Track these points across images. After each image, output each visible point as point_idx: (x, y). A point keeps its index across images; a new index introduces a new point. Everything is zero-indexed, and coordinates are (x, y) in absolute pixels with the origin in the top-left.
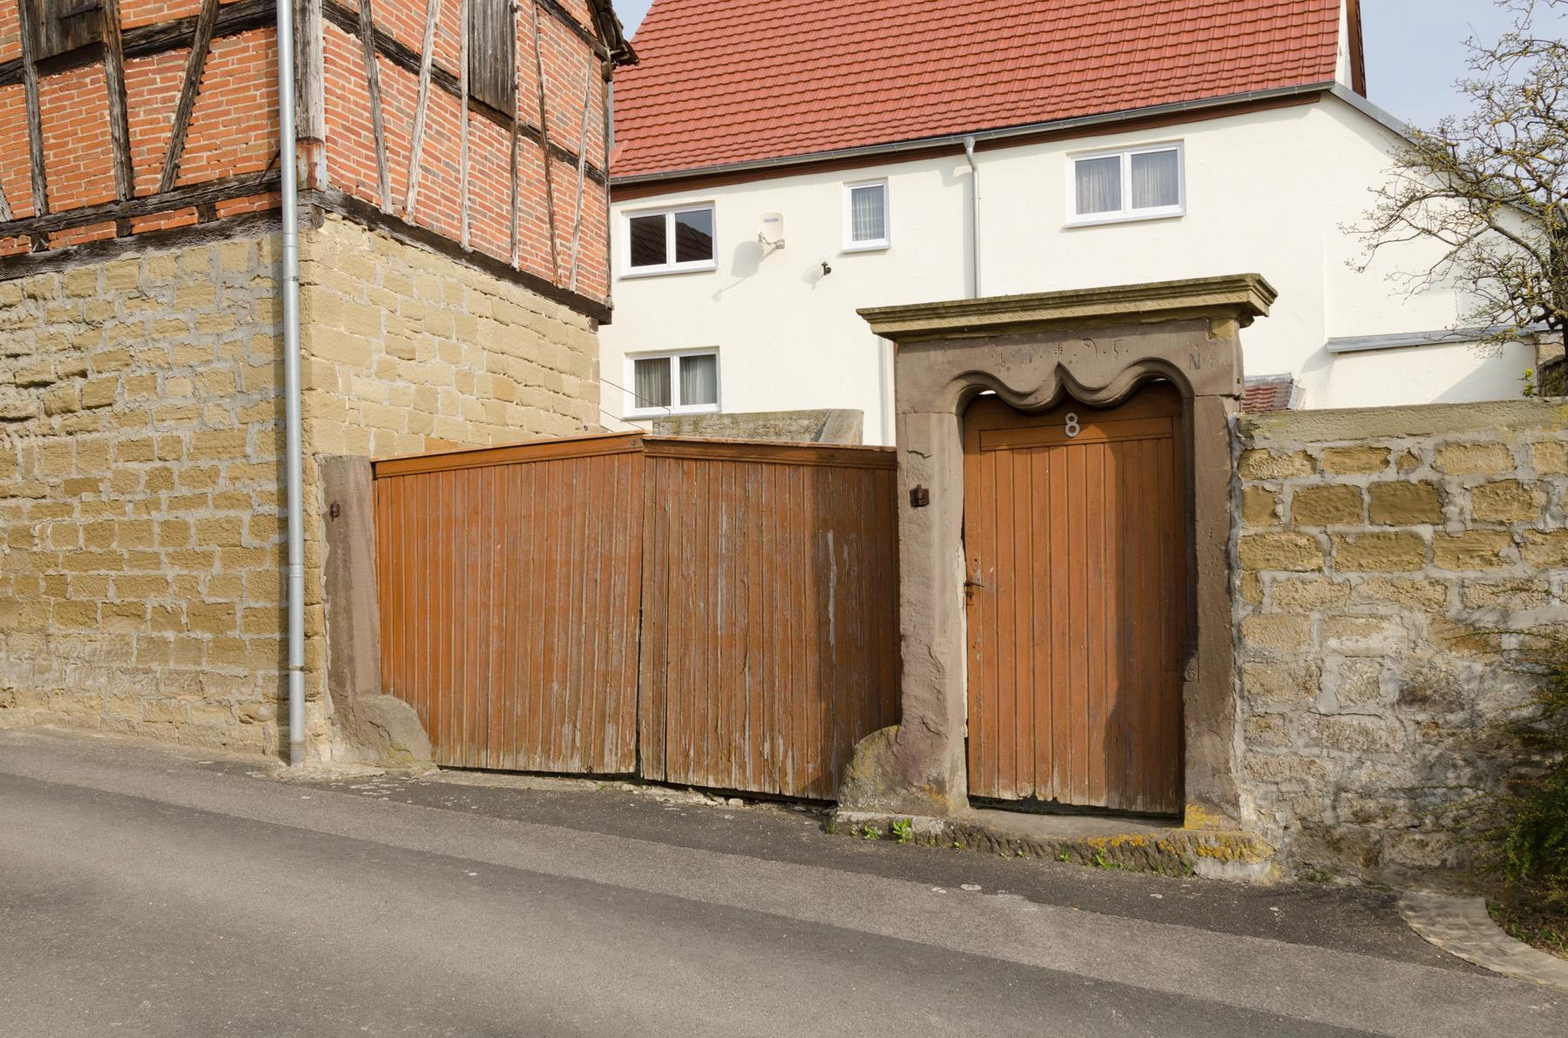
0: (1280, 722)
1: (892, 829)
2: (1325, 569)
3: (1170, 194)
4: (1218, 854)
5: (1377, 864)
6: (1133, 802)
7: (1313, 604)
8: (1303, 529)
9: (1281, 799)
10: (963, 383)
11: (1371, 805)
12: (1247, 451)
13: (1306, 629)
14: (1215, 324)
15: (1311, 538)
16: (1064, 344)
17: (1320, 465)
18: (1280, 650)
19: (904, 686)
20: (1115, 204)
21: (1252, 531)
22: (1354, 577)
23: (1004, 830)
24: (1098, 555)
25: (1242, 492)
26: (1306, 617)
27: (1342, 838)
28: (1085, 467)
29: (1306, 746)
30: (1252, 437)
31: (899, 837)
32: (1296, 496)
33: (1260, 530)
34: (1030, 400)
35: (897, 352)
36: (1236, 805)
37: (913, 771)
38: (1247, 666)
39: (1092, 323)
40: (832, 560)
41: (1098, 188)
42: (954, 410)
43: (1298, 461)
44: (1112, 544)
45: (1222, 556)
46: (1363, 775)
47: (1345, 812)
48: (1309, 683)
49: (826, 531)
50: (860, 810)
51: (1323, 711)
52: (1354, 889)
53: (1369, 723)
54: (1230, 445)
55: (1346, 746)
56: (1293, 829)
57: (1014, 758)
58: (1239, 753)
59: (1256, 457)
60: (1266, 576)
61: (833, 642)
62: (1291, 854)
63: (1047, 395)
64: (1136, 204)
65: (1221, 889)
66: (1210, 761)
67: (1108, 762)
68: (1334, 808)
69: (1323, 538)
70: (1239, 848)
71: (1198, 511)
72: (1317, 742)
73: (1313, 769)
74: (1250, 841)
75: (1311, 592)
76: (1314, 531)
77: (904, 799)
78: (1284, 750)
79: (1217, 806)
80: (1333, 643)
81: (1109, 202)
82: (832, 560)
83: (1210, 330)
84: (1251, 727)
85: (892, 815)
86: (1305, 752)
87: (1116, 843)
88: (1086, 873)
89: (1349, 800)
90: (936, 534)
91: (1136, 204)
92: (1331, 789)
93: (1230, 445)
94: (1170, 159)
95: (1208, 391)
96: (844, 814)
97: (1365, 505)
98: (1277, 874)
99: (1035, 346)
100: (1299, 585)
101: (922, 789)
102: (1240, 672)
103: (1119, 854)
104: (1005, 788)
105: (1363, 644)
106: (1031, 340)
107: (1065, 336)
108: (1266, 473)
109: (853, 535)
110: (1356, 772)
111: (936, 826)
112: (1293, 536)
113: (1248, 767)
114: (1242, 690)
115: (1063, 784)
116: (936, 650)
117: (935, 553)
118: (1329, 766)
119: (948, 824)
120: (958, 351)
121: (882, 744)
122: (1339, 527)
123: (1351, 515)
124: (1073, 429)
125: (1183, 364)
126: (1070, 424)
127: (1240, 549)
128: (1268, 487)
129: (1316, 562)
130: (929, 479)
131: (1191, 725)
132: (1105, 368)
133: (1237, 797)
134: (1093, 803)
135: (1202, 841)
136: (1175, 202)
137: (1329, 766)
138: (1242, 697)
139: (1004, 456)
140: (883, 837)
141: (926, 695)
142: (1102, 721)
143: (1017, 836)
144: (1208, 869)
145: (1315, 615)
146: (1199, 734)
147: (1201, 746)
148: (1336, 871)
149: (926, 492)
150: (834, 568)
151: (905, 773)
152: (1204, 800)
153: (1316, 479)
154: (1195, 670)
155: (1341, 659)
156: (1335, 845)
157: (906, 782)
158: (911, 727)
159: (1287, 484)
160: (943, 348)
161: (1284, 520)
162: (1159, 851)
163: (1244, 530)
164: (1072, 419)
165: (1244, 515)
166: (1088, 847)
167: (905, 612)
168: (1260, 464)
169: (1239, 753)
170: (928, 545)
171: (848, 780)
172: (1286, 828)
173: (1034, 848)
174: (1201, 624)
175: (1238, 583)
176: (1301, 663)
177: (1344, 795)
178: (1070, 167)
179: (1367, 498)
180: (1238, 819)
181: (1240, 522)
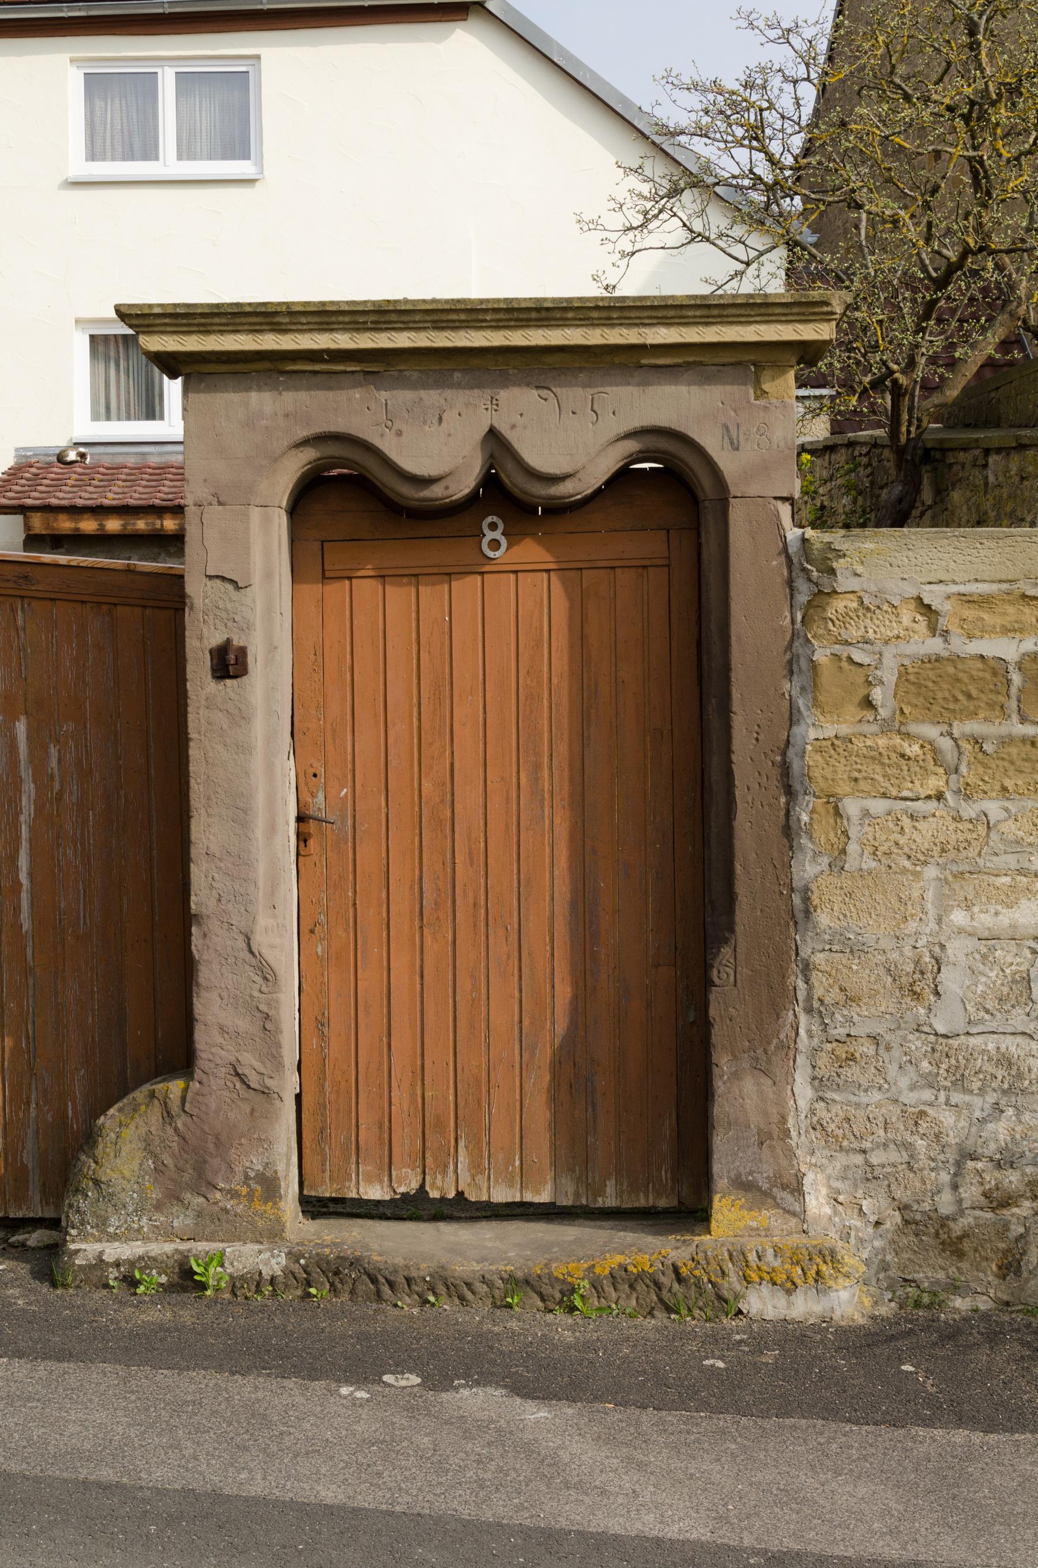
0: (871, 1050)
1: (187, 1273)
2: (948, 795)
3: (236, 138)
4: (781, 1278)
5: (1018, 1272)
6: (600, 1192)
7: (928, 853)
8: (913, 728)
9: (871, 1176)
10: (309, 454)
11: (1013, 1179)
12: (822, 596)
13: (916, 894)
14: (766, 375)
15: (929, 745)
16: (503, 395)
17: (942, 623)
18: (875, 931)
19: (199, 1007)
20: (150, 152)
21: (830, 731)
22: (994, 808)
23: (399, 1261)
24: (537, 767)
25: (814, 666)
26: (917, 875)
27: (965, 1235)
28: (513, 611)
29: (913, 1088)
30: (832, 572)
31: (203, 1286)
32: (903, 673)
33: (844, 729)
34: (436, 491)
35: (186, 390)
36: (798, 1191)
37: (216, 1162)
38: (819, 958)
39: (550, 359)
40: (26, 772)
41: (120, 123)
42: (284, 504)
43: (907, 615)
44: (562, 749)
45: (775, 773)
46: (1001, 1130)
47: (970, 1193)
48: (920, 983)
49: (13, 718)
50: (117, 1236)
51: (941, 1029)
52: (985, 1316)
53: (1012, 1046)
54: (790, 583)
55: (976, 1085)
56: (888, 1225)
57: (386, 1127)
58: (803, 1104)
59: (838, 605)
60: (852, 807)
61: (26, 925)
62: (885, 1267)
63: (464, 485)
64: (185, 152)
65: (793, 1336)
66: (755, 1120)
67: (555, 1126)
68: (955, 1187)
69: (946, 744)
70: (815, 1265)
71: (736, 695)
72: (930, 1082)
73: (923, 1126)
74: (833, 1252)
75: (924, 834)
76: (931, 731)
77: (199, 1215)
78: (876, 1096)
79: (767, 1194)
80: (958, 917)
81: (137, 145)
82: (26, 772)
83: (757, 383)
84: (823, 1059)
85: (184, 1246)
86: (910, 1098)
87: (603, 1270)
88: (562, 1327)
89: (979, 1173)
90: (259, 728)
91: (185, 152)
92: (951, 1156)
93: (790, 583)
94: (238, 84)
95: (752, 490)
96: (85, 1249)
97: (1014, 691)
98: (867, 1302)
99: (448, 393)
100: (906, 821)
101: (234, 1194)
102: (807, 968)
103: (609, 1290)
104: (369, 1180)
105: (1006, 918)
106: (441, 383)
107: (504, 381)
108: (854, 633)
109: (69, 727)
110: (990, 1126)
111: (273, 1262)
112: (897, 740)
113: (818, 1126)
114: (809, 998)
115: (476, 1167)
116: (259, 940)
117: (257, 765)
118: (948, 1118)
119: (294, 1256)
120: (303, 396)
121: (155, 1114)
122: (973, 727)
123: (991, 706)
124: (495, 544)
125: (710, 442)
126: (490, 535)
127: (812, 762)
128: (858, 656)
129: (935, 783)
130: (246, 627)
131: (723, 1062)
132: (573, 439)
133: (799, 1178)
134: (529, 1197)
135: (752, 1257)
136: (245, 156)
137: (948, 1118)
138: (809, 1010)
139: (366, 589)
140: (169, 1288)
141: (243, 1024)
142: (544, 1055)
143: (424, 1269)
144: (763, 1303)
145: (931, 872)
146: (736, 1075)
147: (738, 1094)
148: (954, 1288)
149: (243, 651)
150: (29, 788)
151: (200, 1168)
152: (743, 1185)
153: (935, 645)
154: (726, 968)
155: (971, 943)
156: (954, 1247)
157: (203, 1183)
158: (212, 1087)
159: (889, 652)
160: (275, 387)
161: (883, 713)
162: (680, 1279)
163: (815, 730)
164: (493, 527)
165: (816, 703)
166: (553, 1280)
167: (199, 873)
168: (845, 618)
169: (803, 1104)
170: (244, 749)
171: (87, 1184)
172: (878, 1224)
173: (458, 1290)
174: (741, 889)
175: (805, 818)
176: (908, 951)
177: (970, 1164)
178: (75, 80)
179: (1016, 678)
180: (801, 1215)
181: (809, 716)
